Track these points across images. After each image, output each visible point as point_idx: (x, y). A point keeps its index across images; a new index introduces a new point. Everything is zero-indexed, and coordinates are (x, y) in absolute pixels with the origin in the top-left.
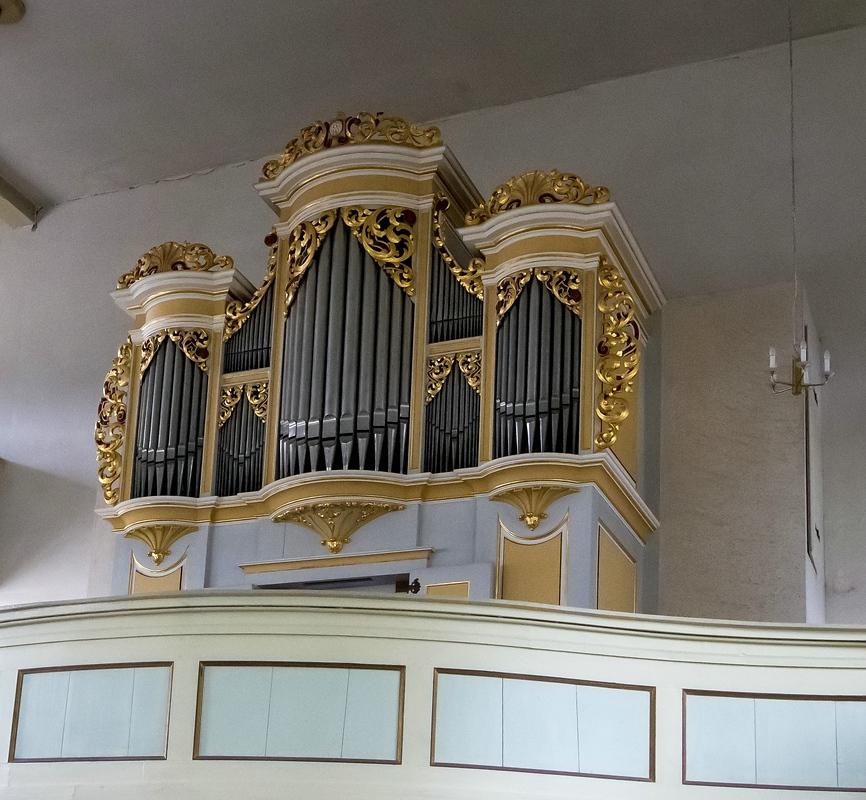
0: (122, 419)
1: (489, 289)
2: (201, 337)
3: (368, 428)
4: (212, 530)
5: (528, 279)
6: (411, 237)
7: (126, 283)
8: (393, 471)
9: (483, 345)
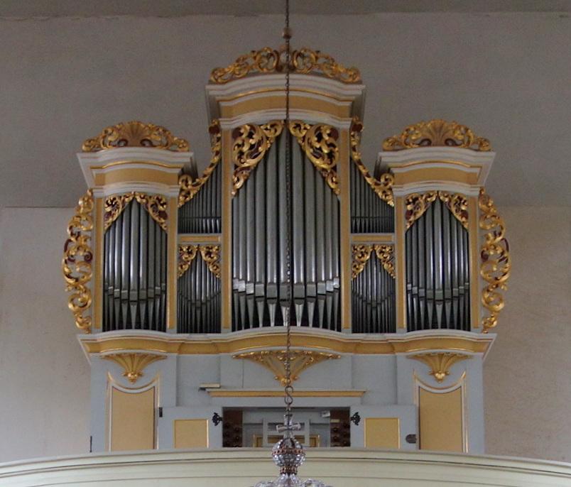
0: (89, 259)
1: (397, 199)
2: (162, 202)
3: (304, 296)
4: (178, 358)
5: (131, 198)
6: (337, 149)
7: (94, 147)
8: (136, 328)
9: (397, 239)
